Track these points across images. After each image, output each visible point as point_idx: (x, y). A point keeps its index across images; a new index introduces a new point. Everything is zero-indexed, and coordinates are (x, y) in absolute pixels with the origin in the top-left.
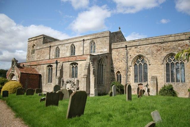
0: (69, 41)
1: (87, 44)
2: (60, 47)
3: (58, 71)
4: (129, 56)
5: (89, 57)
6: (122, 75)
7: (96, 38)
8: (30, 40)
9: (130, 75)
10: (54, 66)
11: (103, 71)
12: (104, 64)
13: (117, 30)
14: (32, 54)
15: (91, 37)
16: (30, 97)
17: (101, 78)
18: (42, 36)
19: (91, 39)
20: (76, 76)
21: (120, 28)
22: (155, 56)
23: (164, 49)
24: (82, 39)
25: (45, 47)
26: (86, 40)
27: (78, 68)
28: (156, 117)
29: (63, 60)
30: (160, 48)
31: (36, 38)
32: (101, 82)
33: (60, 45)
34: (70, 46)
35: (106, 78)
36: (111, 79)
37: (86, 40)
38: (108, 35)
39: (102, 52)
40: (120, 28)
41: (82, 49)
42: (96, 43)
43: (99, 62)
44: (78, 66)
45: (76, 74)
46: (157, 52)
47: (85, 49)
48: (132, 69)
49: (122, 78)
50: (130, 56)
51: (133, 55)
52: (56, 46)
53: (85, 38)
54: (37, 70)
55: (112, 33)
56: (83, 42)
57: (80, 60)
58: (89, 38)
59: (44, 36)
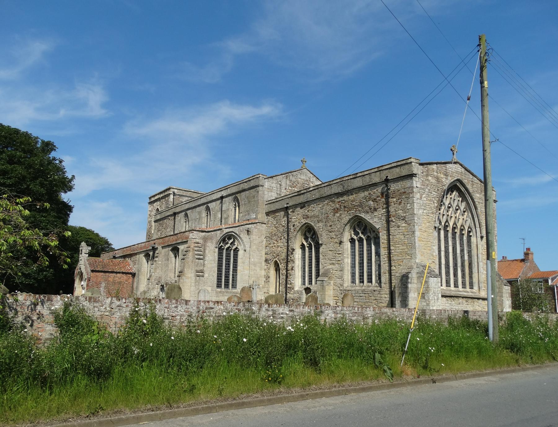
4: (291, 225)
9: (292, 269)
22: (331, 223)
23: (345, 207)
30: (338, 206)
46: (334, 215)
48: (298, 254)
50: (294, 226)
51: (298, 224)
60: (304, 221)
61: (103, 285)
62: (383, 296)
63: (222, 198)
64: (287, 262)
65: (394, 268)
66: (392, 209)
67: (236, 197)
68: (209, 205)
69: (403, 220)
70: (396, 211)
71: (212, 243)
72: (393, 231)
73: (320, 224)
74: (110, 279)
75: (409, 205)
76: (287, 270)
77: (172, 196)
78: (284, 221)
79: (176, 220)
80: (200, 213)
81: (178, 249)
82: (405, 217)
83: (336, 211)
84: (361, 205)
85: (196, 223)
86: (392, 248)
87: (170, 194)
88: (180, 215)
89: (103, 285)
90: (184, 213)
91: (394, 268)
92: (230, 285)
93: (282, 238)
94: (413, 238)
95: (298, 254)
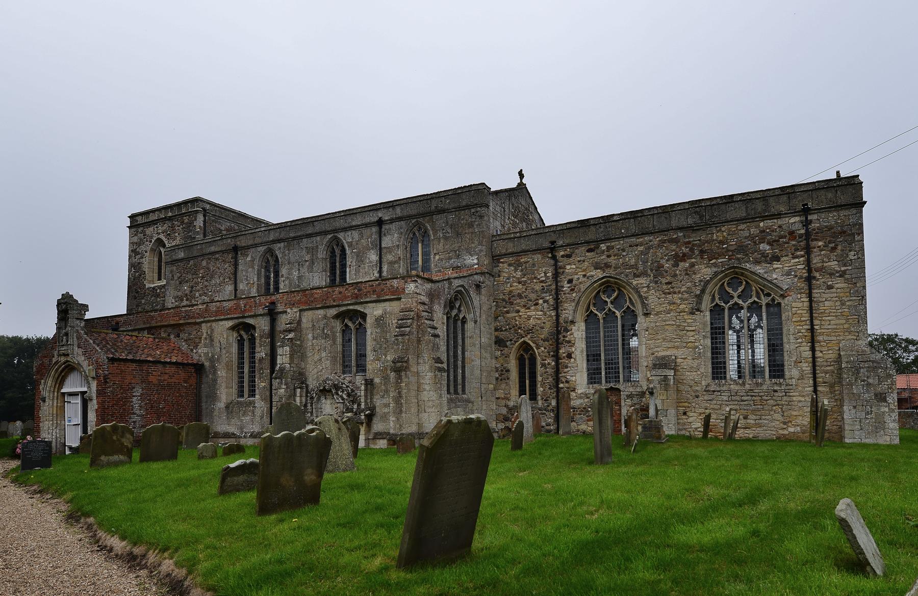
6: (539, 358)
7: (431, 214)
11: (467, 341)
12: (470, 317)
17: (460, 371)
21: (521, 175)
27: (369, 332)
32: (460, 387)
37: (392, 221)
40: (521, 175)
48: (578, 333)
49: (539, 369)
60: (599, 274)
61: (138, 391)
62: (794, 399)
63: (380, 223)
64: (557, 345)
65: (820, 355)
66: (816, 260)
67: (419, 226)
68: (341, 236)
69: (841, 276)
70: (823, 262)
71: (439, 304)
72: (816, 295)
73: (643, 281)
74: (151, 378)
75: (852, 253)
76: (557, 358)
77: (200, 218)
78: (545, 272)
79: (241, 261)
80: (312, 251)
81: (364, 316)
82: (844, 272)
83: (678, 259)
84: (741, 248)
85: (304, 270)
86: (816, 322)
87: (197, 212)
88: (251, 252)
89: (138, 391)
90: (262, 249)
91: (820, 355)
92: (621, 380)
93: (541, 301)
94: (862, 307)
95: (578, 333)
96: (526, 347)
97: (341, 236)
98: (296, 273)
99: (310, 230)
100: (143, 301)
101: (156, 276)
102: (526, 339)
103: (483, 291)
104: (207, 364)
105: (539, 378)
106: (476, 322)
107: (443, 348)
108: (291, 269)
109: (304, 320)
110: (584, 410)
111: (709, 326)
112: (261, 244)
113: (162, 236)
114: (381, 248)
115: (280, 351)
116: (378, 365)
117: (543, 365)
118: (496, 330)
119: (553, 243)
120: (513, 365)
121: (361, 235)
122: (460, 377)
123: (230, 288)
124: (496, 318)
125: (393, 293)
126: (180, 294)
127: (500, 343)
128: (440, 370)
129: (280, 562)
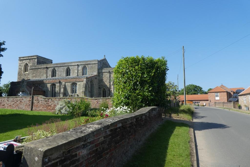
0: (65, 65)
1: (80, 68)
2: (56, 69)
3: (62, 88)
5: (85, 80)
6: (106, 91)
7: (88, 64)
8: (21, 59)
10: (57, 85)
11: (94, 88)
12: (94, 84)
13: (103, 58)
14: (24, 72)
15: (84, 63)
16: (4, 105)
17: (92, 93)
18: (36, 57)
19: (84, 65)
20: (76, 92)
21: (105, 56)
24: (77, 64)
25: (42, 67)
26: (80, 65)
27: (77, 86)
28: (33, 124)
29: (65, 81)
31: (30, 58)
32: (92, 96)
33: (57, 67)
34: (66, 69)
35: (95, 93)
36: (99, 94)
37: (80, 65)
38: (97, 62)
39: (92, 74)
40: (105, 56)
41: (76, 71)
42: (87, 67)
43: (91, 82)
44: (77, 85)
45: (76, 90)
47: (79, 72)
49: (106, 93)
52: (53, 68)
53: (79, 64)
54: (41, 88)
55: (100, 61)
56: (77, 66)
57: (79, 81)
58: (81, 63)
59: (38, 57)
68: (70, 67)
96: (104, 89)
97: (70, 67)
98: (60, 73)
99: (63, 65)
100: (22, 76)
101: (25, 71)
102: (104, 88)
103: (97, 79)
104: (46, 91)
105: (106, 94)
106: (95, 84)
107: (90, 89)
108: (59, 72)
109: (66, 84)
110: (75, 70)
111: (56, 86)
112: (52, 67)
113: (27, 63)
114: (78, 70)
115: (61, 89)
116: (79, 92)
117: (107, 92)
118: (99, 86)
119: (109, 71)
120: (102, 92)
121: (74, 67)
122: (92, 94)
123: (45, 75)
124: (99, 84)
125: (82, 80)
126: (33, 76)
127: (99, 88)
128: (90, 93)
129: (94, 87)
